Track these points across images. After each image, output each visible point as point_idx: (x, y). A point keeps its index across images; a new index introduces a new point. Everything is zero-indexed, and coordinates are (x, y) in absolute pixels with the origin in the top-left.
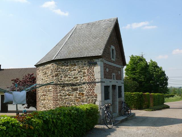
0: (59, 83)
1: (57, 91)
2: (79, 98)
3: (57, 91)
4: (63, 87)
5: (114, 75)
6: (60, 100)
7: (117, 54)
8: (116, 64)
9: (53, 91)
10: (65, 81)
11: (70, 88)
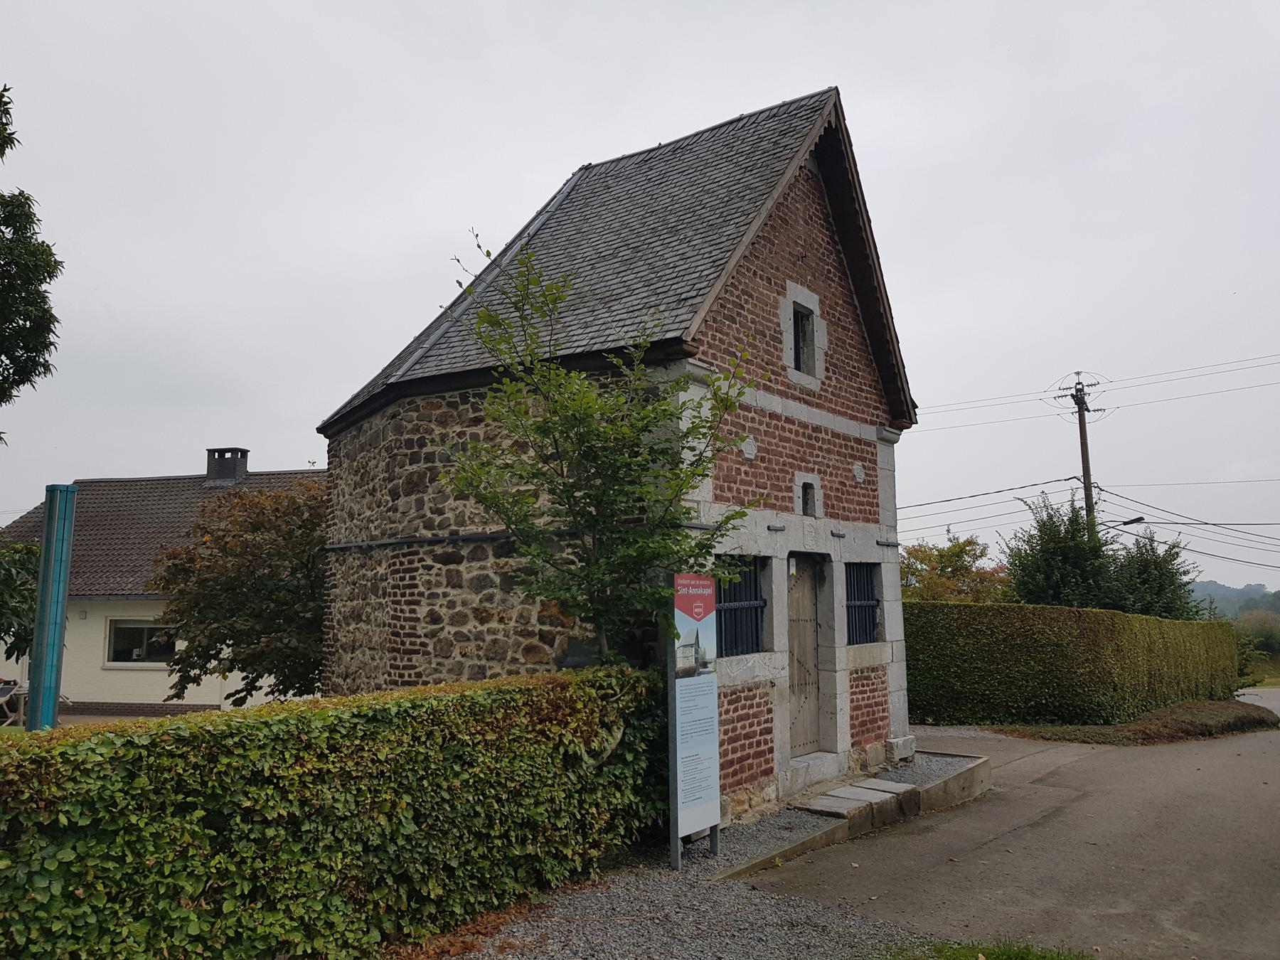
0: (428, 534)
1: (416, 586)
2: (543, 636)
3: (416, 586)
4: (446, 559)
5: (807, 487)
6: (430, 649)
7: (836, 342)
8: (834, 411)
9: (393, 587)
10: (462, 524)
11: (490, 565)
